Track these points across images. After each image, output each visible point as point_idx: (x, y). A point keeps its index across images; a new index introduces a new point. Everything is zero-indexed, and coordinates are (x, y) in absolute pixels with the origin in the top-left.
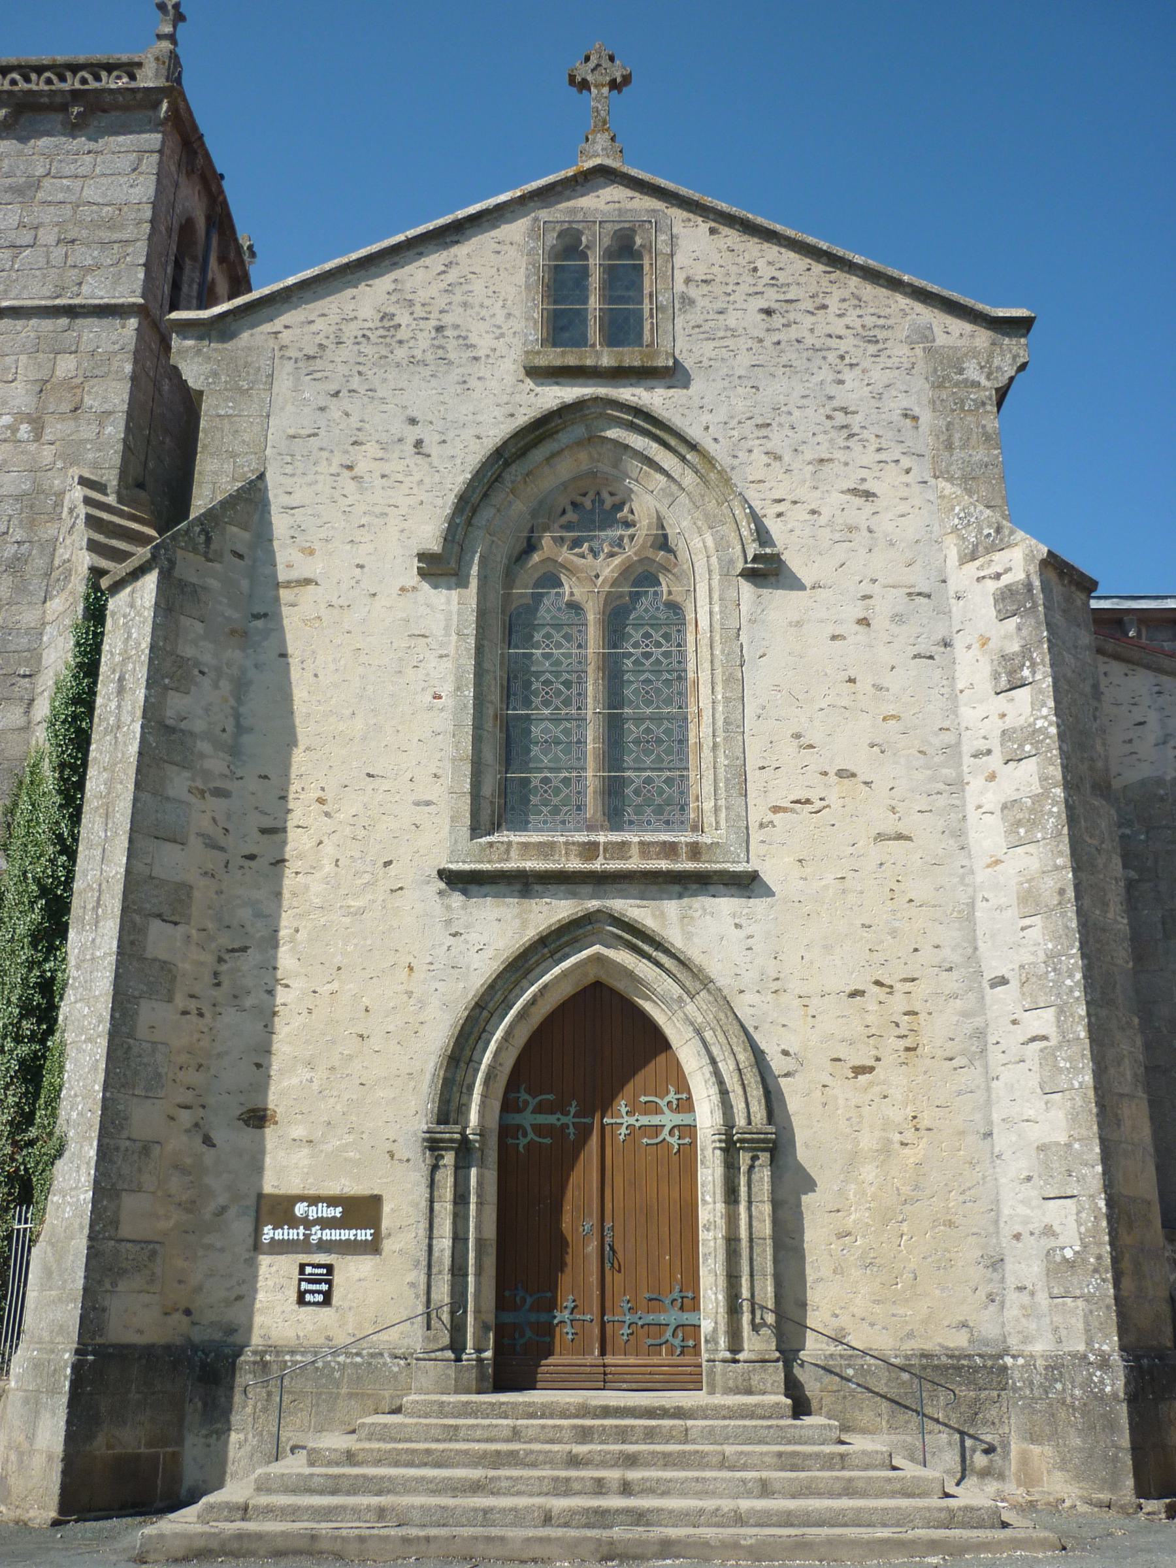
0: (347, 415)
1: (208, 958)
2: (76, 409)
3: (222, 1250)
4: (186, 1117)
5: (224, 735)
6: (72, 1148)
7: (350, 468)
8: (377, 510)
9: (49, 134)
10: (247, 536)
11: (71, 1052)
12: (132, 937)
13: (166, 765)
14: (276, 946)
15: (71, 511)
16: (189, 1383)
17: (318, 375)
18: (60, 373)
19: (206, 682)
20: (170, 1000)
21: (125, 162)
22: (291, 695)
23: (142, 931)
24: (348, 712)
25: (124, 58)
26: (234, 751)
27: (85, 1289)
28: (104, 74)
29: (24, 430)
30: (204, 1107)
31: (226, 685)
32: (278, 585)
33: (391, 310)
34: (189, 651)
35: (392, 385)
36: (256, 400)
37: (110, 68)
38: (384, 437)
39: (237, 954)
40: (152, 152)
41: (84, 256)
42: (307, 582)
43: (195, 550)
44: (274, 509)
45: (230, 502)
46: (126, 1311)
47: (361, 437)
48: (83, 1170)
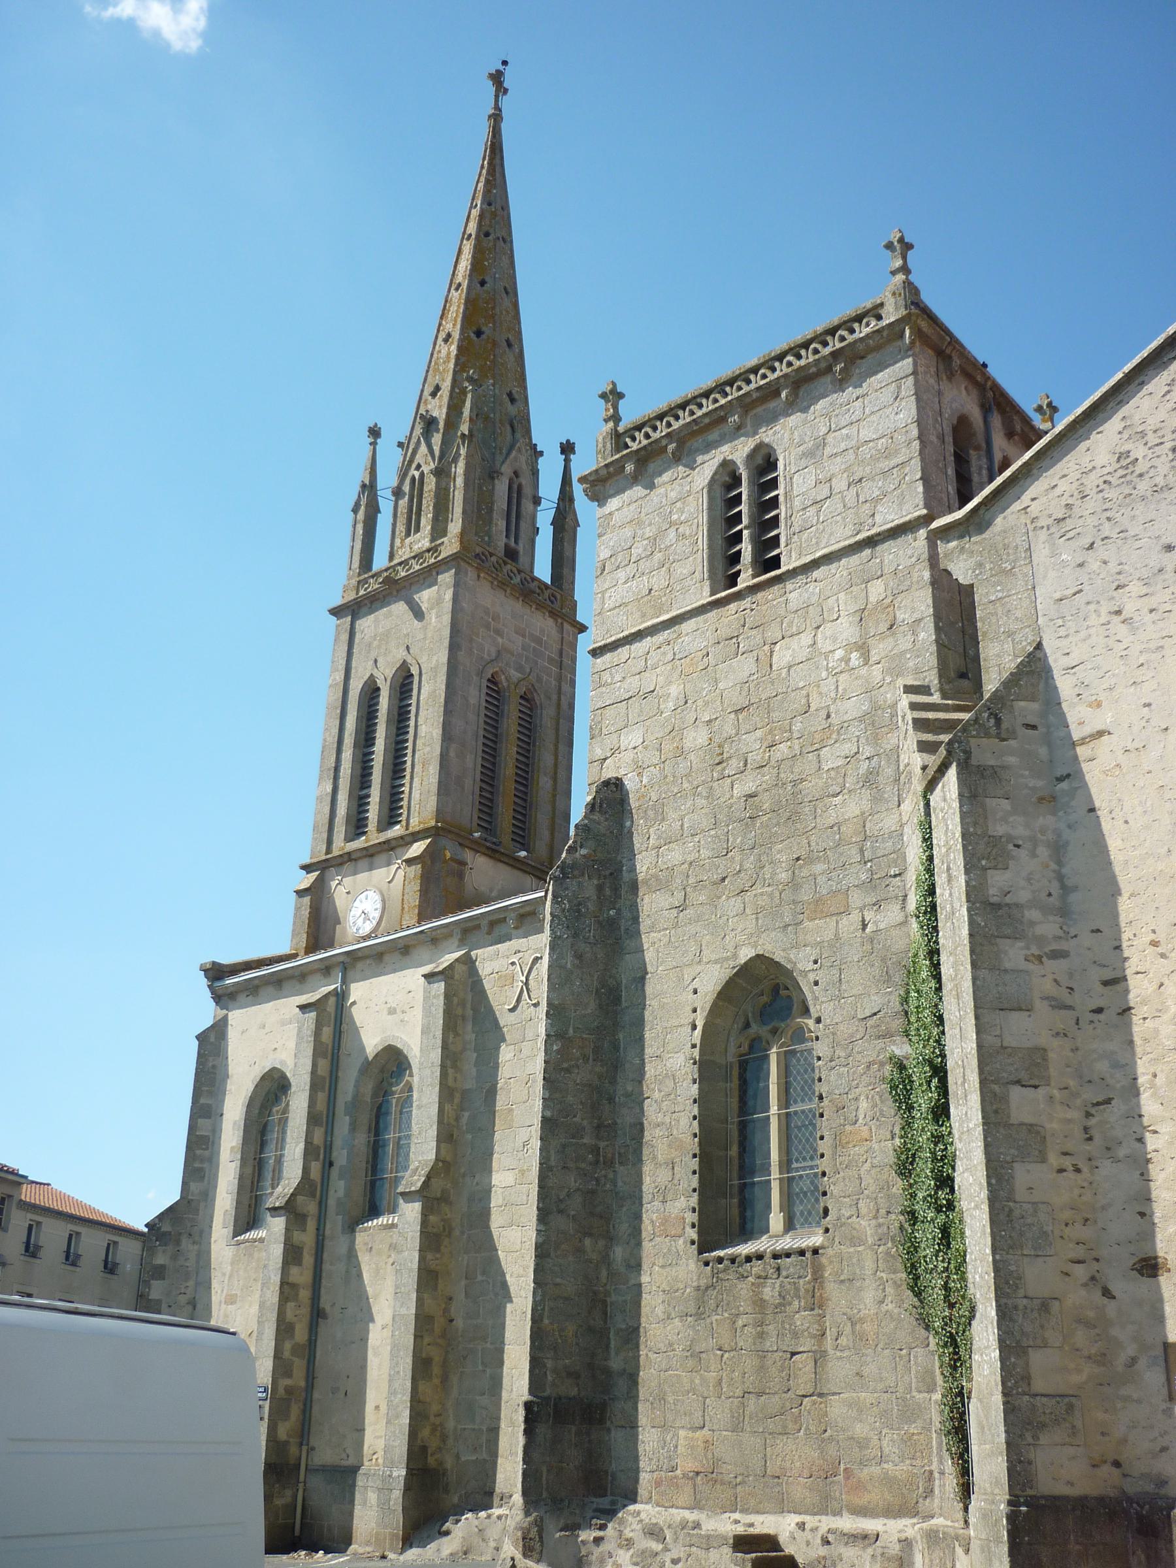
0: (1105, 563)
1: (1075, 1114)
2: (892, 626)
3: (1139, 1401)
4: (1080, 1271)
5: (1051, 899)
6: (980, 1308)
7: (1118, 613)
8: (1153, 645)
9: (824, 396)
10: (1035, 706)
11: (967, 1219)
12: (994, 1107)
13: (998, 940)
14: (1137, 1094)
15: (903, 717)
16: (1130, 1536)
17: (1069, 535)
18: (873, 599)
19: (1023, 854)
20: (1043, 1160)
21: (887, 395)
22: (1106, 846)
23: (1004, 1099)
24: (1164, 850)
25: (869, 305)
26: (1064, 912)
27: (1008, 1443)
28: (856, 326)
29: (855, 655)
30: (1097, 1260)
31: (1043, 852)
32: (1074, 744)
33: (1126, 447)
34: (999, 830)
35: (1141, 520)
36: (1020, 576)
37: (859, 319)
38: (1145, 573)
39: (1102, 1107)
40: (907, 376)
41: (871, 490)
42: (1100, 734)
43: (987, 735)
44: (1056, 674)
45: (1012, 681)
46: (1052, 1464)
47: (1122, 579)
48: (990, 1326)
